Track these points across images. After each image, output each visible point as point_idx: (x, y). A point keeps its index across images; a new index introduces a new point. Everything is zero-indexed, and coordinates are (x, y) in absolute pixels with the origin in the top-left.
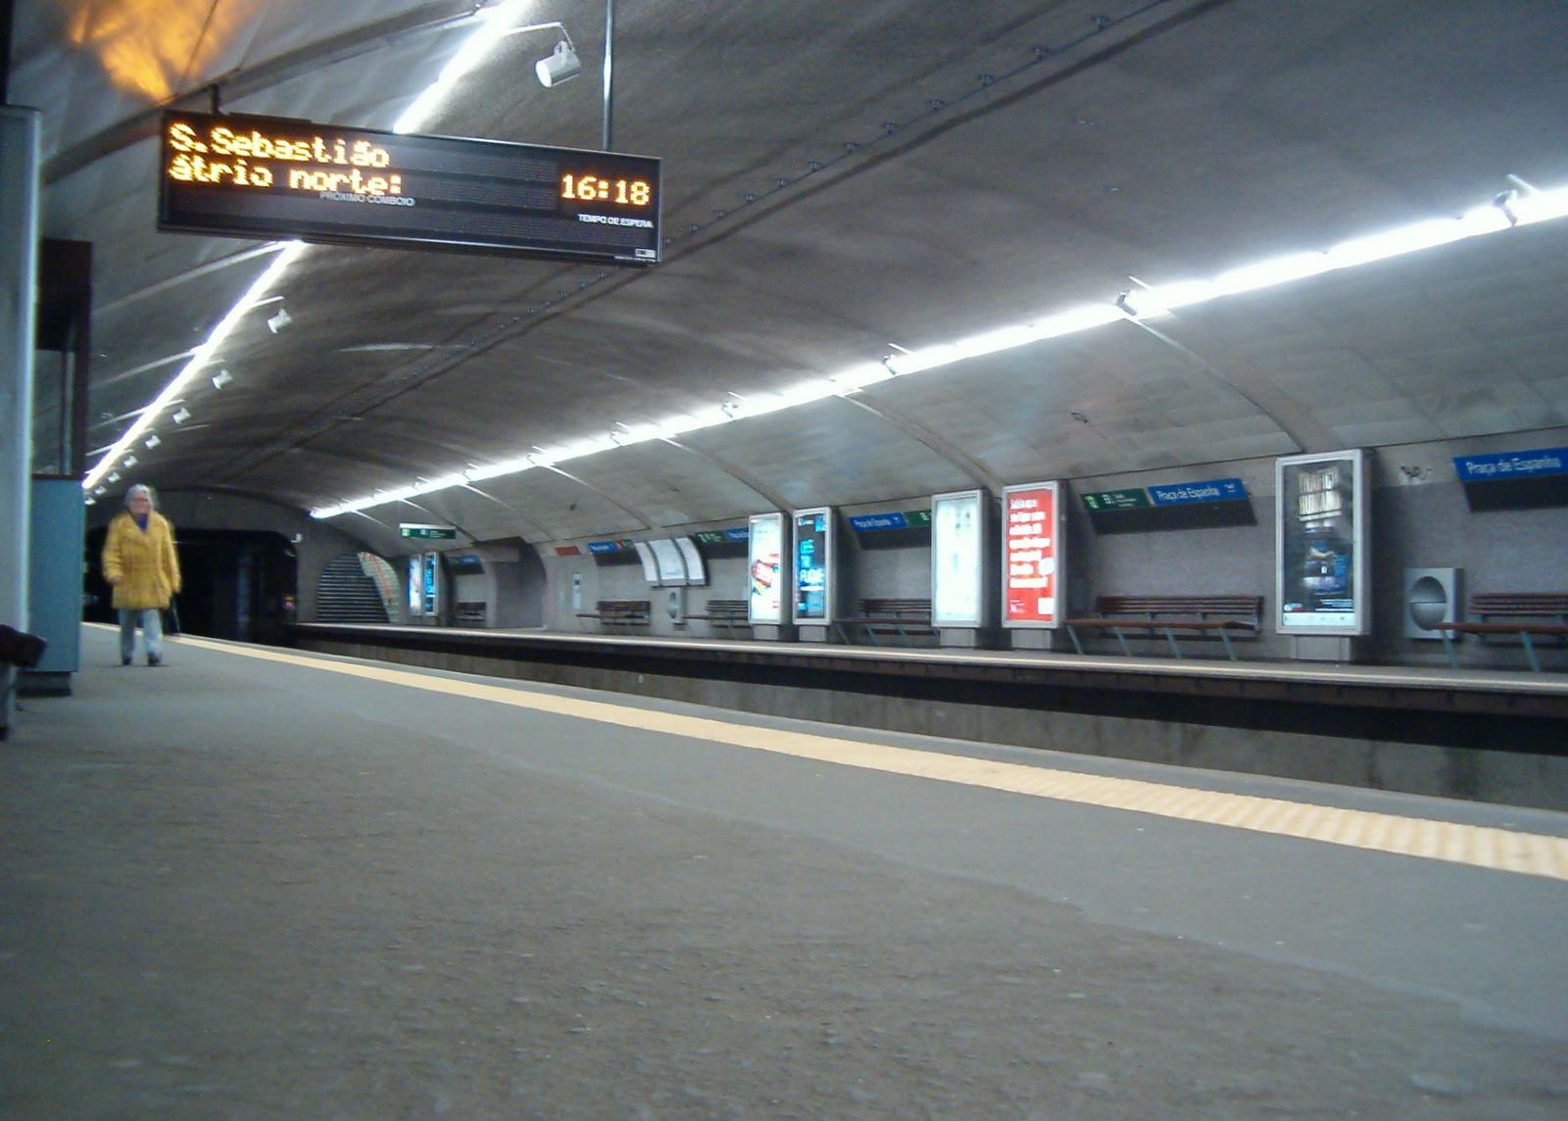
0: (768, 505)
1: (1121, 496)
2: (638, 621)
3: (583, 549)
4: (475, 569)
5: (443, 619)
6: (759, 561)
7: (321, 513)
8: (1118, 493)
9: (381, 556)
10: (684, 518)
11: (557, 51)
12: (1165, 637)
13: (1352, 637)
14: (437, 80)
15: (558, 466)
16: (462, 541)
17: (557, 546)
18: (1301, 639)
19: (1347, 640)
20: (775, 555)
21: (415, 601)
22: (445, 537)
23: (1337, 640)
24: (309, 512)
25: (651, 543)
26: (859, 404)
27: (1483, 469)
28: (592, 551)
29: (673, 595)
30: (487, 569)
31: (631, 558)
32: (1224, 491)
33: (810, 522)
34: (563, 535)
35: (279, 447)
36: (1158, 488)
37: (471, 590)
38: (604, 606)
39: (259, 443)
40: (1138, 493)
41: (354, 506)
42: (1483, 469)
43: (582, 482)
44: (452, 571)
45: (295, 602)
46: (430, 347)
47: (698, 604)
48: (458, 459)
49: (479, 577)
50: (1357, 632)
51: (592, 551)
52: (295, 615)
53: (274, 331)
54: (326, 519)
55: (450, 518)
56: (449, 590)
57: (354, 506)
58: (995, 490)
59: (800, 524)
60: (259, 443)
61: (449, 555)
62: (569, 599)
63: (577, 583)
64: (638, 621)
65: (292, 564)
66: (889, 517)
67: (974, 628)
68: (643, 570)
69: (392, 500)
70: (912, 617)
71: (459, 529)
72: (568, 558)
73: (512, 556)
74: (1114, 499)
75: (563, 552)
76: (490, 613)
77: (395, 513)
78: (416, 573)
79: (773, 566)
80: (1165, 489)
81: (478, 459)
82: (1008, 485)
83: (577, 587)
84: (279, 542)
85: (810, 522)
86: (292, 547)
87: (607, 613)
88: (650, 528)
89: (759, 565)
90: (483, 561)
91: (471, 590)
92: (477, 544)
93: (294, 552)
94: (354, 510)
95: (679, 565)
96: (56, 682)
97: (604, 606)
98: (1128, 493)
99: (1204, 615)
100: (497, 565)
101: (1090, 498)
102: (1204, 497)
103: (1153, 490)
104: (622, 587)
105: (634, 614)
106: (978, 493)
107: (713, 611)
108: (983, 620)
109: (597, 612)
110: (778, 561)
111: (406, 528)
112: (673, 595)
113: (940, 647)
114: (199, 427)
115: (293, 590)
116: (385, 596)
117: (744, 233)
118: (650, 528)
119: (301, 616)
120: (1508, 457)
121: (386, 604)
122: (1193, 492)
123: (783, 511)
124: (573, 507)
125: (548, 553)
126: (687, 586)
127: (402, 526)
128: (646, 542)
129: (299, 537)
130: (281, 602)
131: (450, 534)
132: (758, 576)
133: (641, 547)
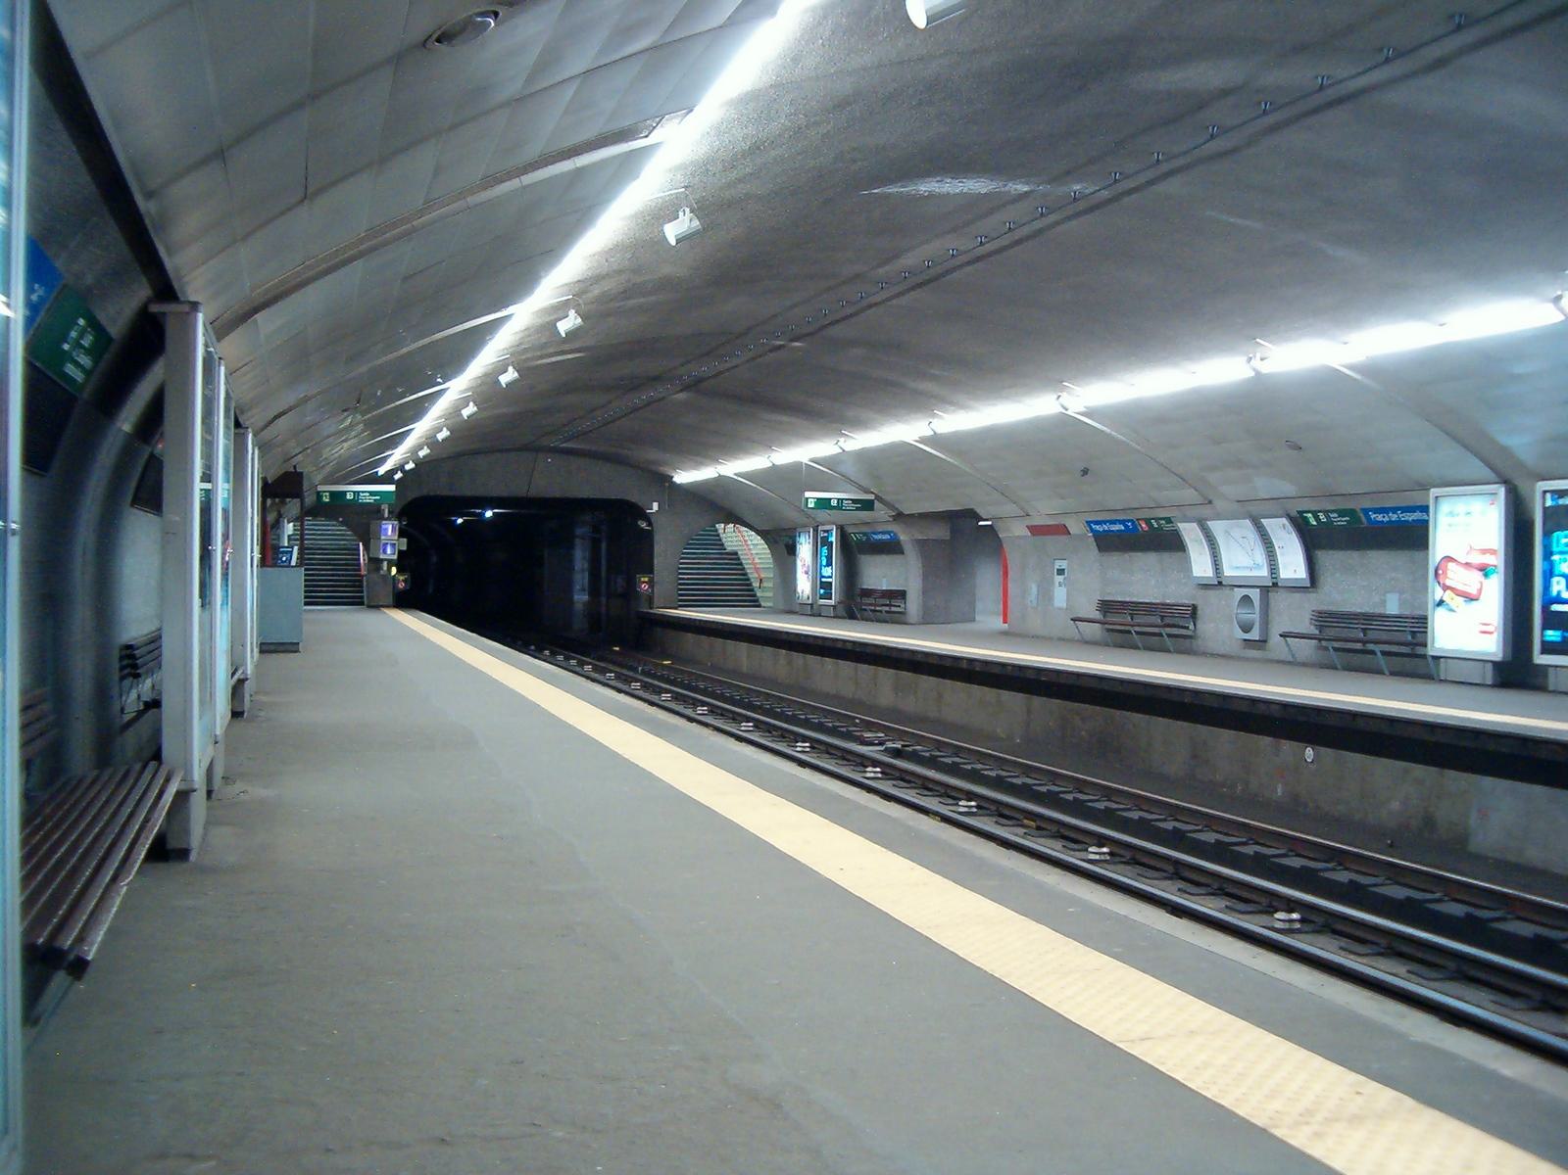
0: (1481, 470)
1: (1336, 515)
2: (893, 609)
3: (1076, 527)
4: (892, 548)
5: (841, 611)
6: (1449, 559)
7: (683, 477)
8: (1333, 511)
9: (751, 528)
10: (1287, 488)
11: (681, 214)
12: (1373, 653)
13: (1495, 664)
14: (638, 177)
15: (923, 440)
16: (881, 513)
17: (1030, 524)
18: (1449, 660)
19: (1490, 664)
20: (1493, 552)
21: (804, 586)
22: (857, 509)
23: (1482, 663)
24: (672, 477)
25: (1264, 521)
26: (740, 479)
27: (1380, 518)
28: (1092, 530)
29: (1246, 599)
30: (908, 548)
31: (1164, 541)
32: (1126, 526)
33: (826, 534)
34: (1044, 511)
35: (660, 391)
36: (1092, 522)
37: (878, 574)
38: (1106, 606)
39: (634, 385)
40: (1351, 513)
41: (734, 467)
42: (1380, 518)
43: (1108, 431)
44: (853, 550)
45: (651, 583)
46: (1026, 189)
47: (1294, 615)
48: (921, 403)
49: (896, 559)
50: (1499, 657)
51: (1092, 530)
52: (650, 599)
53: (673, 242)
54: (941, 434)
55: (864, 483)
56: (850, 573)
57: (734, 467)
58: (1523, 486)
59: (1549, 503)
60: (634, 385)
61: (850, 530)
62: (1046, 594)
63: (1061, 572)
64: (893, 609)
65: (647, 537)
66: (1122, 522)
67: (1492, 662)
68: (1187, 561)
69: (953, 430)
70: (1384, 636)
71: (878, 498)
72: (1049, 539)
73: (941, 532)
74: (1328, 517)
75: (1037, 530)
76: (913, 605)
77: (795, 478)
78: (805, 549)
79: (1484, 569)
80: (1097, 523)
81: (951, 403)
82: (1543, 480)
83: (1060, 578)
84: (638, 512)
85: (826, 534)
86: (647, 518)
87: (1110, 618)
88: (1210, 502)
89: (1451, 565)
90: (902, 538)
91: (878, 574)
92: (899, 516)
93: (650, 524)
94: (805, 460)
95: (1260, 557)
96: (270, 561)
97: (1106, 606)
98: (1342, 513)
99: (1162, 617)
100: (922, 545)
101: (1310, 515)
102: (1413, 520)
103: (1366, 511)
104: (1143, 580)
105: (1167, 627)
106: (1502, 490)
107: (1321, 628)
108: (1504, 651)
109: (1098, 615)
110: (1498, 561)
111: (812, 496)
112: (1246, 599)
113: (906, 624)
114: (570, 356)
115: (649, 570)
116: (753, 575)
117: (894, 302)
118: (1210, 502)
119: (656, 602)
120: (1394, 510)
121: (756, 584)
122: (1404, 514)
123: (1505, 482)
124: (1085, 472)
125: (1015, 531)
126: (1272, 587)
127: (808, 494)
128: (1202, 525)
129: (655, 506)
130: (632, 584)
131: (867, 505)
132: (1448, 583)
133: (1190, 532)
